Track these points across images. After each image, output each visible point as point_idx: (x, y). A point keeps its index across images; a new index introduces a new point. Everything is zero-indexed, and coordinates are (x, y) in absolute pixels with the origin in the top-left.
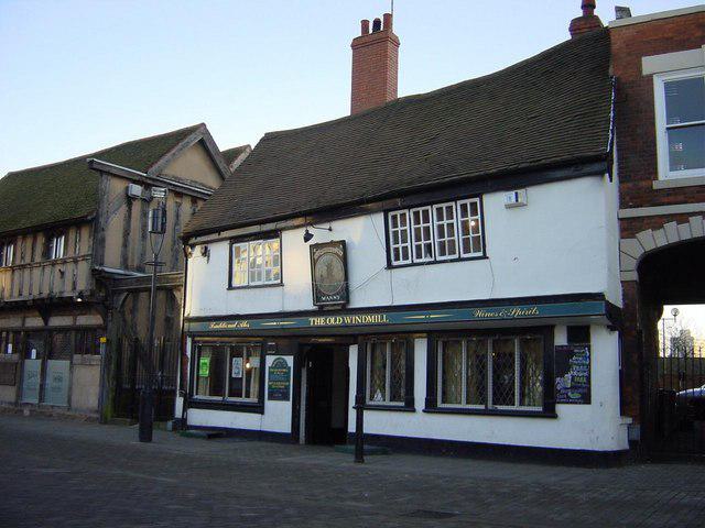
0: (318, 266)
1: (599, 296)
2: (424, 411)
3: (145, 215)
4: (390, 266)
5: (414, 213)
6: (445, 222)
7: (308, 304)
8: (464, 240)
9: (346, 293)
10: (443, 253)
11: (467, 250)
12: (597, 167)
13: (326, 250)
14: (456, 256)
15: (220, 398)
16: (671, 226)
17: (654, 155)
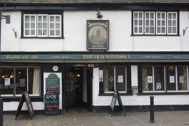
0: (91, 30)
1: (109, 49)
4: (132, 35)
5: (169, 14)
6: (161, 19)
7: (83, 48)
9: (107, 44)
13: (96, 24)
14: (165, 34)
15: (12, 95)
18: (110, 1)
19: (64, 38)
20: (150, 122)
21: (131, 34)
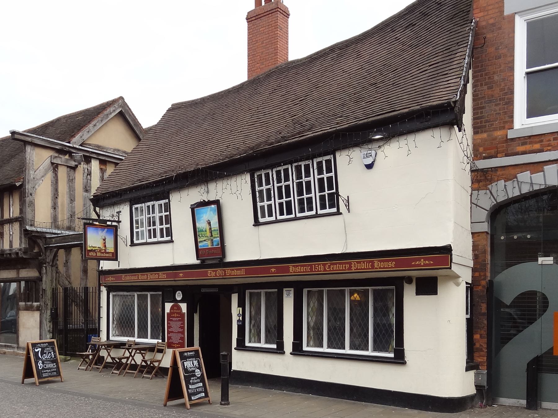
2: (291, 354)
3: (71, 181)
4: (257, 223)
8: (320, 196)
10: (302, 210)
11: (323, 207)
12: (447, 117)
16: (524, 176)
17: (511, 102)
18: (197, 165)
19: (341, 214)
20: (221, 404)
21: (253, 222)
